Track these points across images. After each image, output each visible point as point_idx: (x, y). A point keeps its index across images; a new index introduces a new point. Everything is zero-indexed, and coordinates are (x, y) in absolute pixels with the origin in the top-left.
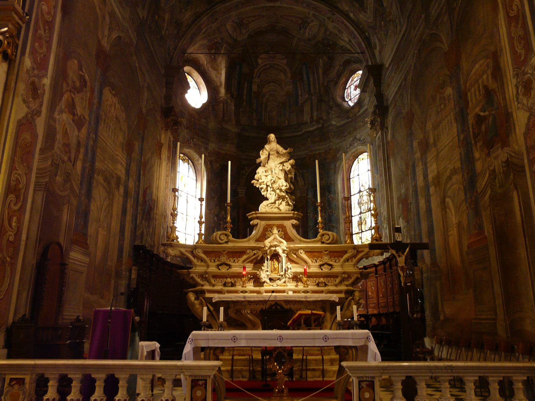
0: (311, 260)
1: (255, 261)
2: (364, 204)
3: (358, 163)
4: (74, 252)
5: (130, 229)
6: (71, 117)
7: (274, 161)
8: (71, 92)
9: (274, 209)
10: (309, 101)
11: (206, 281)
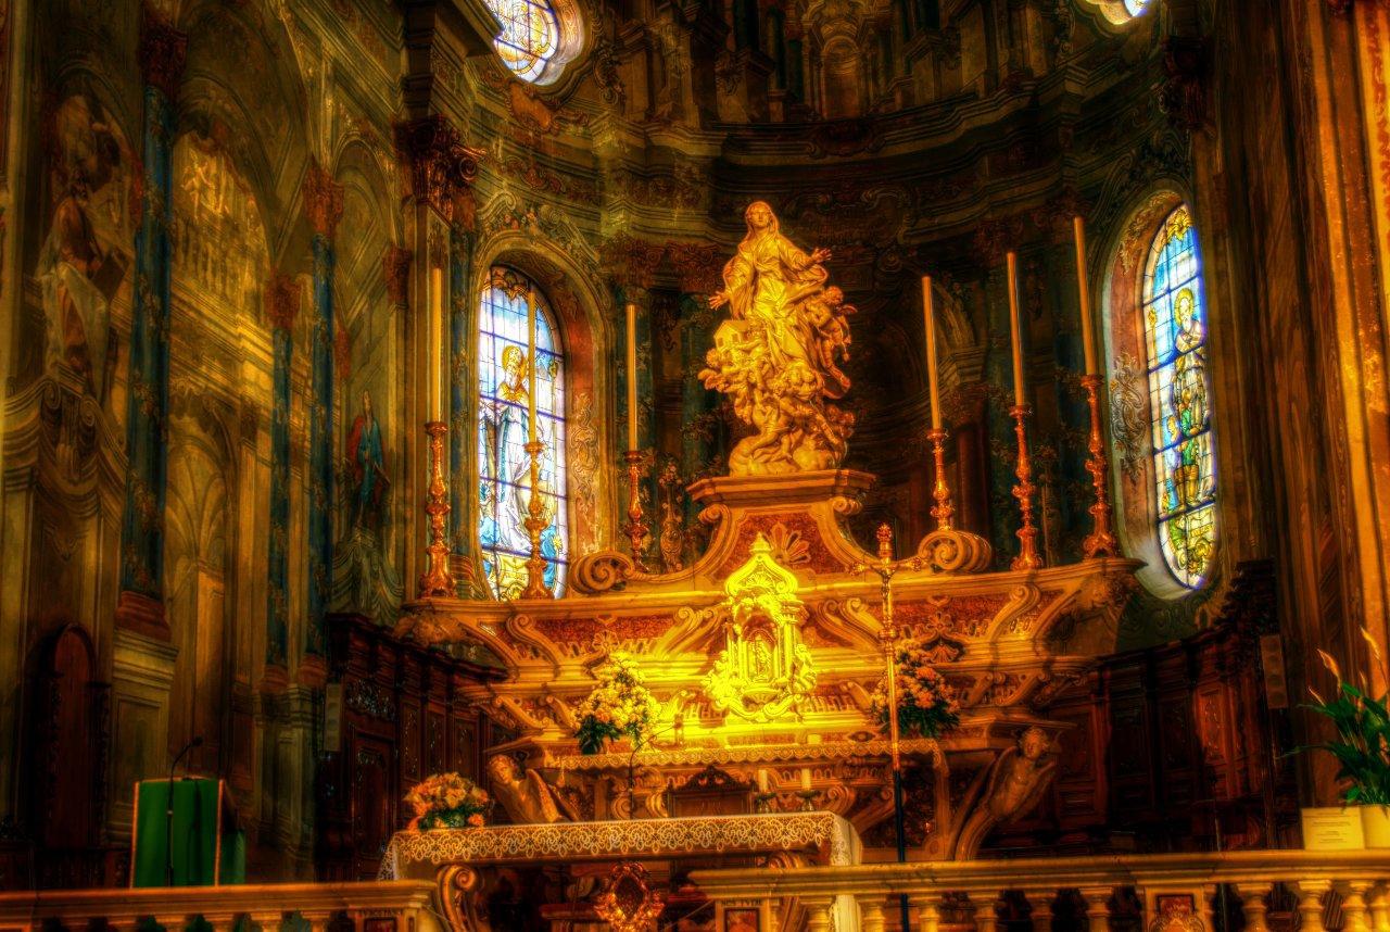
4: (128, 649)
5: (306, 560)
6: (83, 265)
8: (74, 196)
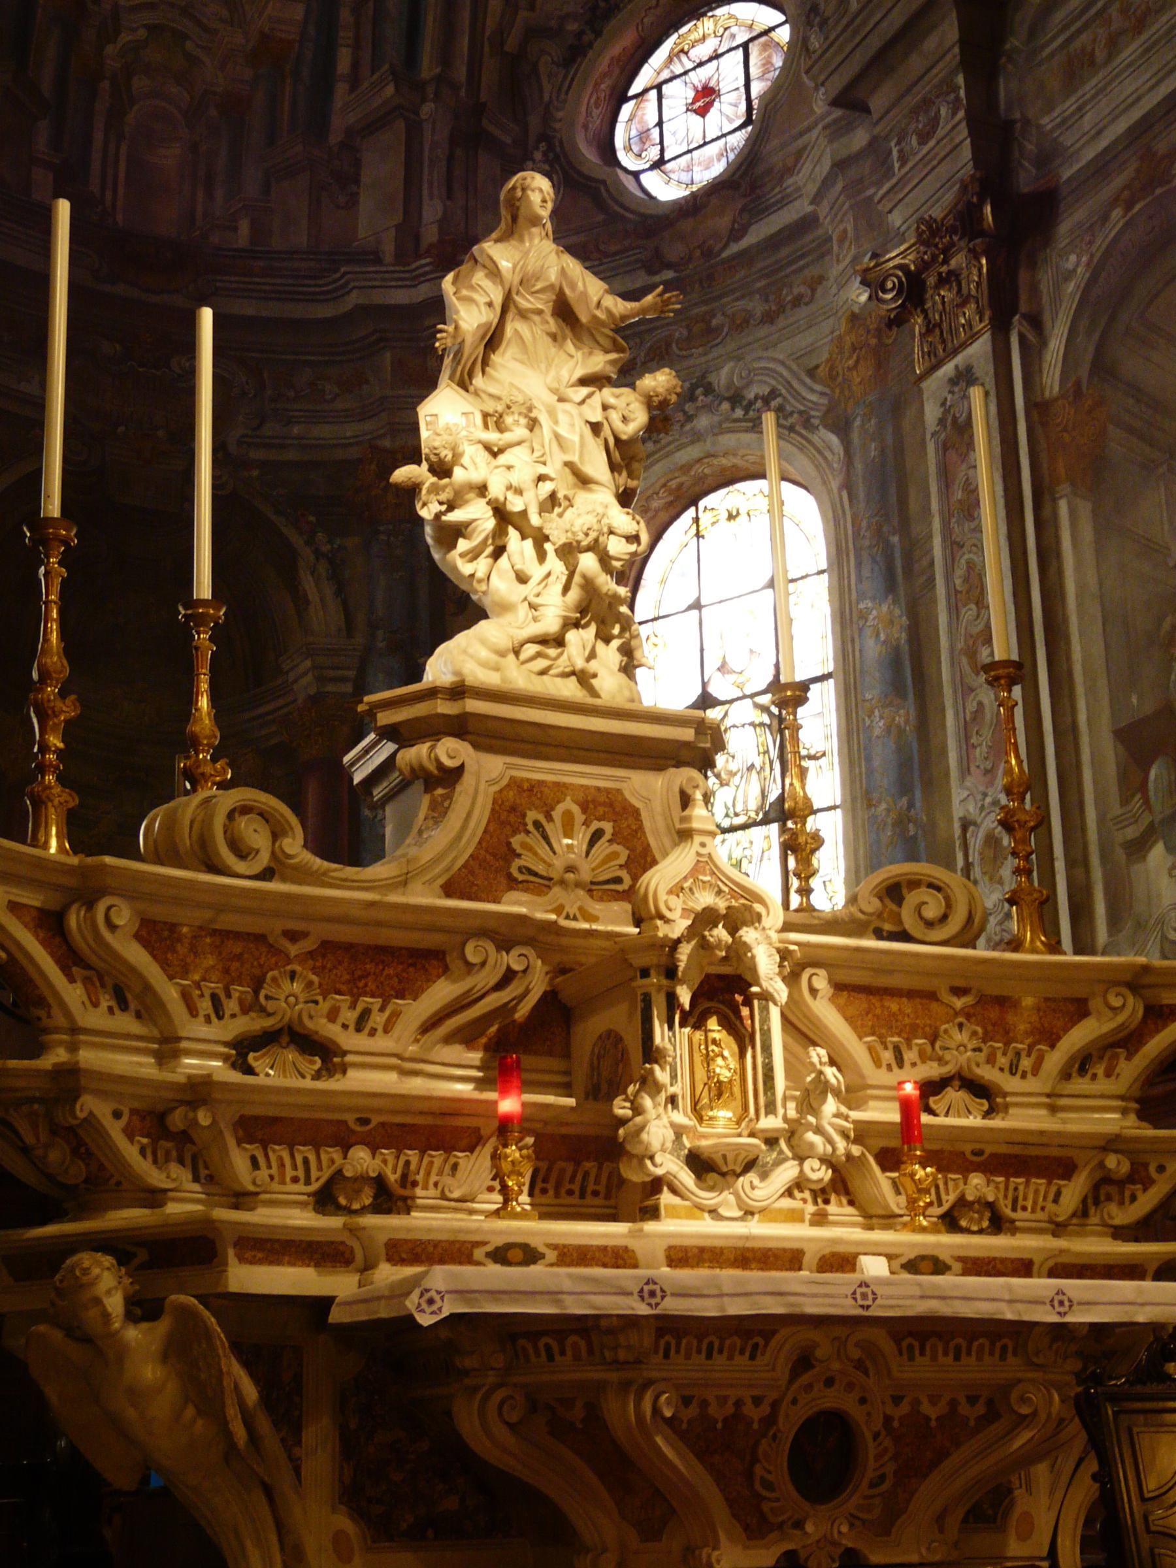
0: (871, 1049)
1: (493, 1029)
2: (736, 780)
3: (698, 535)
7: (528, 356)
9: (559, 680)
10: (400, 125)
11: (181, 1162)
